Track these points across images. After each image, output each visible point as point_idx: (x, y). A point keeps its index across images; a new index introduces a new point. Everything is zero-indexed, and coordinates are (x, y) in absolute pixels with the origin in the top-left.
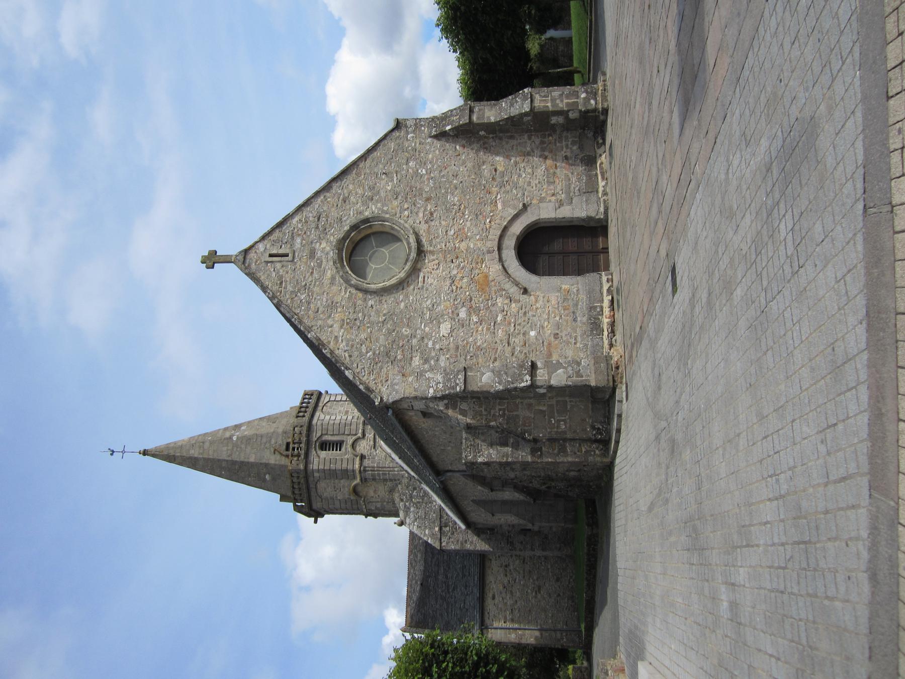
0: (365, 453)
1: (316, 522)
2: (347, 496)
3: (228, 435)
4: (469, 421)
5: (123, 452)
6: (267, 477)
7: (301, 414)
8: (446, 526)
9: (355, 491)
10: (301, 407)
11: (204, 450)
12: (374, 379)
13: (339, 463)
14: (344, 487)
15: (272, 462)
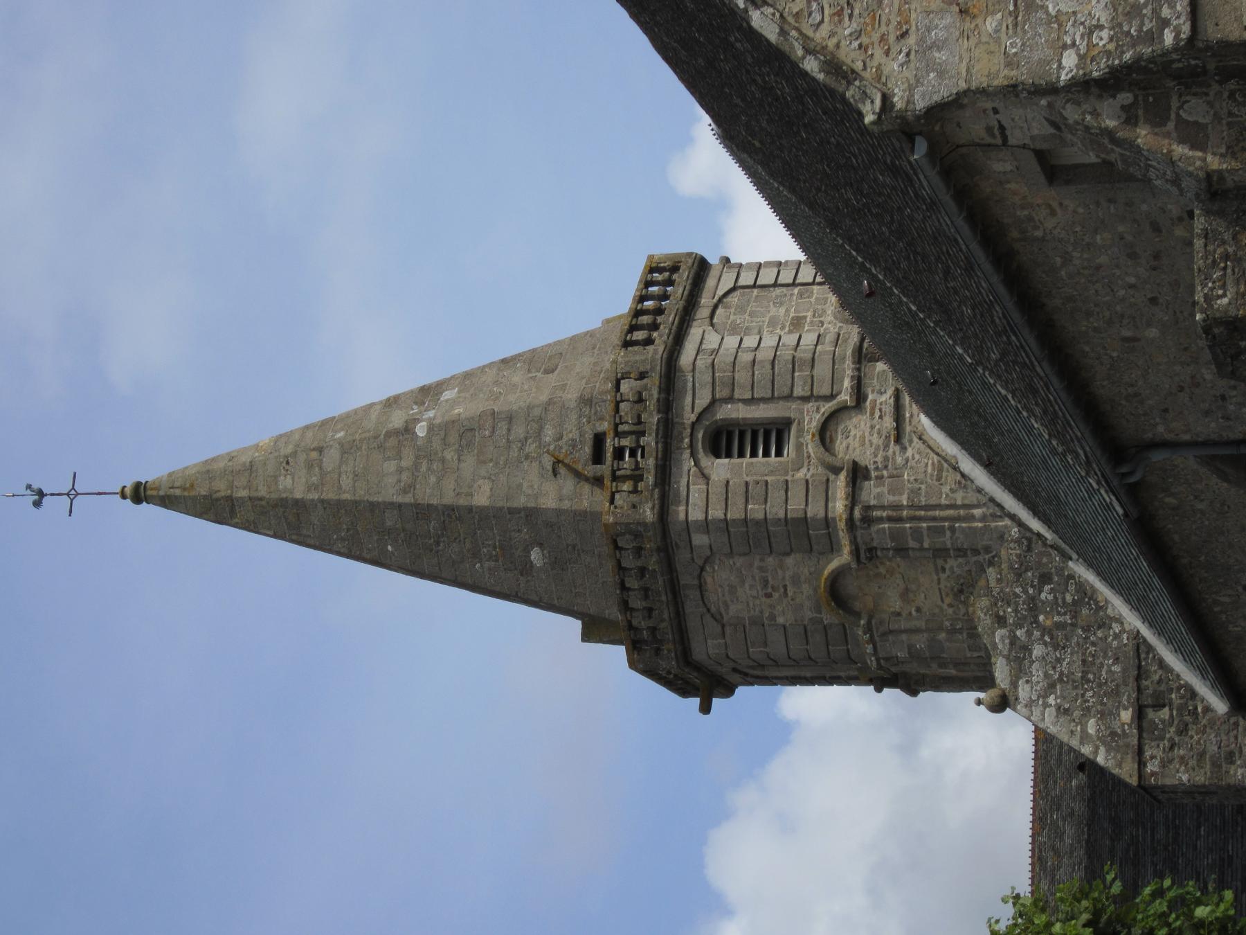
0: (866, 458)
1: (706, 708)
2: (809, 614)
3: (397, 419)
4: (1214, 163)
5: (72, 494)
6: (535, 556)
7: (639, 335)
8: (1158, 706)
9: (836, 593)
10: (637, 313)
11: (323, 474)
12: (858, 34)
13: (776, 496)
14: (796, 580)
15: (549, 502)
